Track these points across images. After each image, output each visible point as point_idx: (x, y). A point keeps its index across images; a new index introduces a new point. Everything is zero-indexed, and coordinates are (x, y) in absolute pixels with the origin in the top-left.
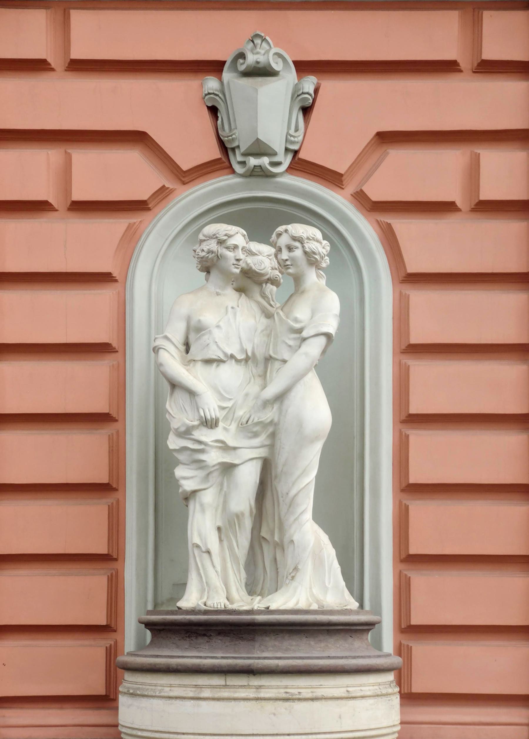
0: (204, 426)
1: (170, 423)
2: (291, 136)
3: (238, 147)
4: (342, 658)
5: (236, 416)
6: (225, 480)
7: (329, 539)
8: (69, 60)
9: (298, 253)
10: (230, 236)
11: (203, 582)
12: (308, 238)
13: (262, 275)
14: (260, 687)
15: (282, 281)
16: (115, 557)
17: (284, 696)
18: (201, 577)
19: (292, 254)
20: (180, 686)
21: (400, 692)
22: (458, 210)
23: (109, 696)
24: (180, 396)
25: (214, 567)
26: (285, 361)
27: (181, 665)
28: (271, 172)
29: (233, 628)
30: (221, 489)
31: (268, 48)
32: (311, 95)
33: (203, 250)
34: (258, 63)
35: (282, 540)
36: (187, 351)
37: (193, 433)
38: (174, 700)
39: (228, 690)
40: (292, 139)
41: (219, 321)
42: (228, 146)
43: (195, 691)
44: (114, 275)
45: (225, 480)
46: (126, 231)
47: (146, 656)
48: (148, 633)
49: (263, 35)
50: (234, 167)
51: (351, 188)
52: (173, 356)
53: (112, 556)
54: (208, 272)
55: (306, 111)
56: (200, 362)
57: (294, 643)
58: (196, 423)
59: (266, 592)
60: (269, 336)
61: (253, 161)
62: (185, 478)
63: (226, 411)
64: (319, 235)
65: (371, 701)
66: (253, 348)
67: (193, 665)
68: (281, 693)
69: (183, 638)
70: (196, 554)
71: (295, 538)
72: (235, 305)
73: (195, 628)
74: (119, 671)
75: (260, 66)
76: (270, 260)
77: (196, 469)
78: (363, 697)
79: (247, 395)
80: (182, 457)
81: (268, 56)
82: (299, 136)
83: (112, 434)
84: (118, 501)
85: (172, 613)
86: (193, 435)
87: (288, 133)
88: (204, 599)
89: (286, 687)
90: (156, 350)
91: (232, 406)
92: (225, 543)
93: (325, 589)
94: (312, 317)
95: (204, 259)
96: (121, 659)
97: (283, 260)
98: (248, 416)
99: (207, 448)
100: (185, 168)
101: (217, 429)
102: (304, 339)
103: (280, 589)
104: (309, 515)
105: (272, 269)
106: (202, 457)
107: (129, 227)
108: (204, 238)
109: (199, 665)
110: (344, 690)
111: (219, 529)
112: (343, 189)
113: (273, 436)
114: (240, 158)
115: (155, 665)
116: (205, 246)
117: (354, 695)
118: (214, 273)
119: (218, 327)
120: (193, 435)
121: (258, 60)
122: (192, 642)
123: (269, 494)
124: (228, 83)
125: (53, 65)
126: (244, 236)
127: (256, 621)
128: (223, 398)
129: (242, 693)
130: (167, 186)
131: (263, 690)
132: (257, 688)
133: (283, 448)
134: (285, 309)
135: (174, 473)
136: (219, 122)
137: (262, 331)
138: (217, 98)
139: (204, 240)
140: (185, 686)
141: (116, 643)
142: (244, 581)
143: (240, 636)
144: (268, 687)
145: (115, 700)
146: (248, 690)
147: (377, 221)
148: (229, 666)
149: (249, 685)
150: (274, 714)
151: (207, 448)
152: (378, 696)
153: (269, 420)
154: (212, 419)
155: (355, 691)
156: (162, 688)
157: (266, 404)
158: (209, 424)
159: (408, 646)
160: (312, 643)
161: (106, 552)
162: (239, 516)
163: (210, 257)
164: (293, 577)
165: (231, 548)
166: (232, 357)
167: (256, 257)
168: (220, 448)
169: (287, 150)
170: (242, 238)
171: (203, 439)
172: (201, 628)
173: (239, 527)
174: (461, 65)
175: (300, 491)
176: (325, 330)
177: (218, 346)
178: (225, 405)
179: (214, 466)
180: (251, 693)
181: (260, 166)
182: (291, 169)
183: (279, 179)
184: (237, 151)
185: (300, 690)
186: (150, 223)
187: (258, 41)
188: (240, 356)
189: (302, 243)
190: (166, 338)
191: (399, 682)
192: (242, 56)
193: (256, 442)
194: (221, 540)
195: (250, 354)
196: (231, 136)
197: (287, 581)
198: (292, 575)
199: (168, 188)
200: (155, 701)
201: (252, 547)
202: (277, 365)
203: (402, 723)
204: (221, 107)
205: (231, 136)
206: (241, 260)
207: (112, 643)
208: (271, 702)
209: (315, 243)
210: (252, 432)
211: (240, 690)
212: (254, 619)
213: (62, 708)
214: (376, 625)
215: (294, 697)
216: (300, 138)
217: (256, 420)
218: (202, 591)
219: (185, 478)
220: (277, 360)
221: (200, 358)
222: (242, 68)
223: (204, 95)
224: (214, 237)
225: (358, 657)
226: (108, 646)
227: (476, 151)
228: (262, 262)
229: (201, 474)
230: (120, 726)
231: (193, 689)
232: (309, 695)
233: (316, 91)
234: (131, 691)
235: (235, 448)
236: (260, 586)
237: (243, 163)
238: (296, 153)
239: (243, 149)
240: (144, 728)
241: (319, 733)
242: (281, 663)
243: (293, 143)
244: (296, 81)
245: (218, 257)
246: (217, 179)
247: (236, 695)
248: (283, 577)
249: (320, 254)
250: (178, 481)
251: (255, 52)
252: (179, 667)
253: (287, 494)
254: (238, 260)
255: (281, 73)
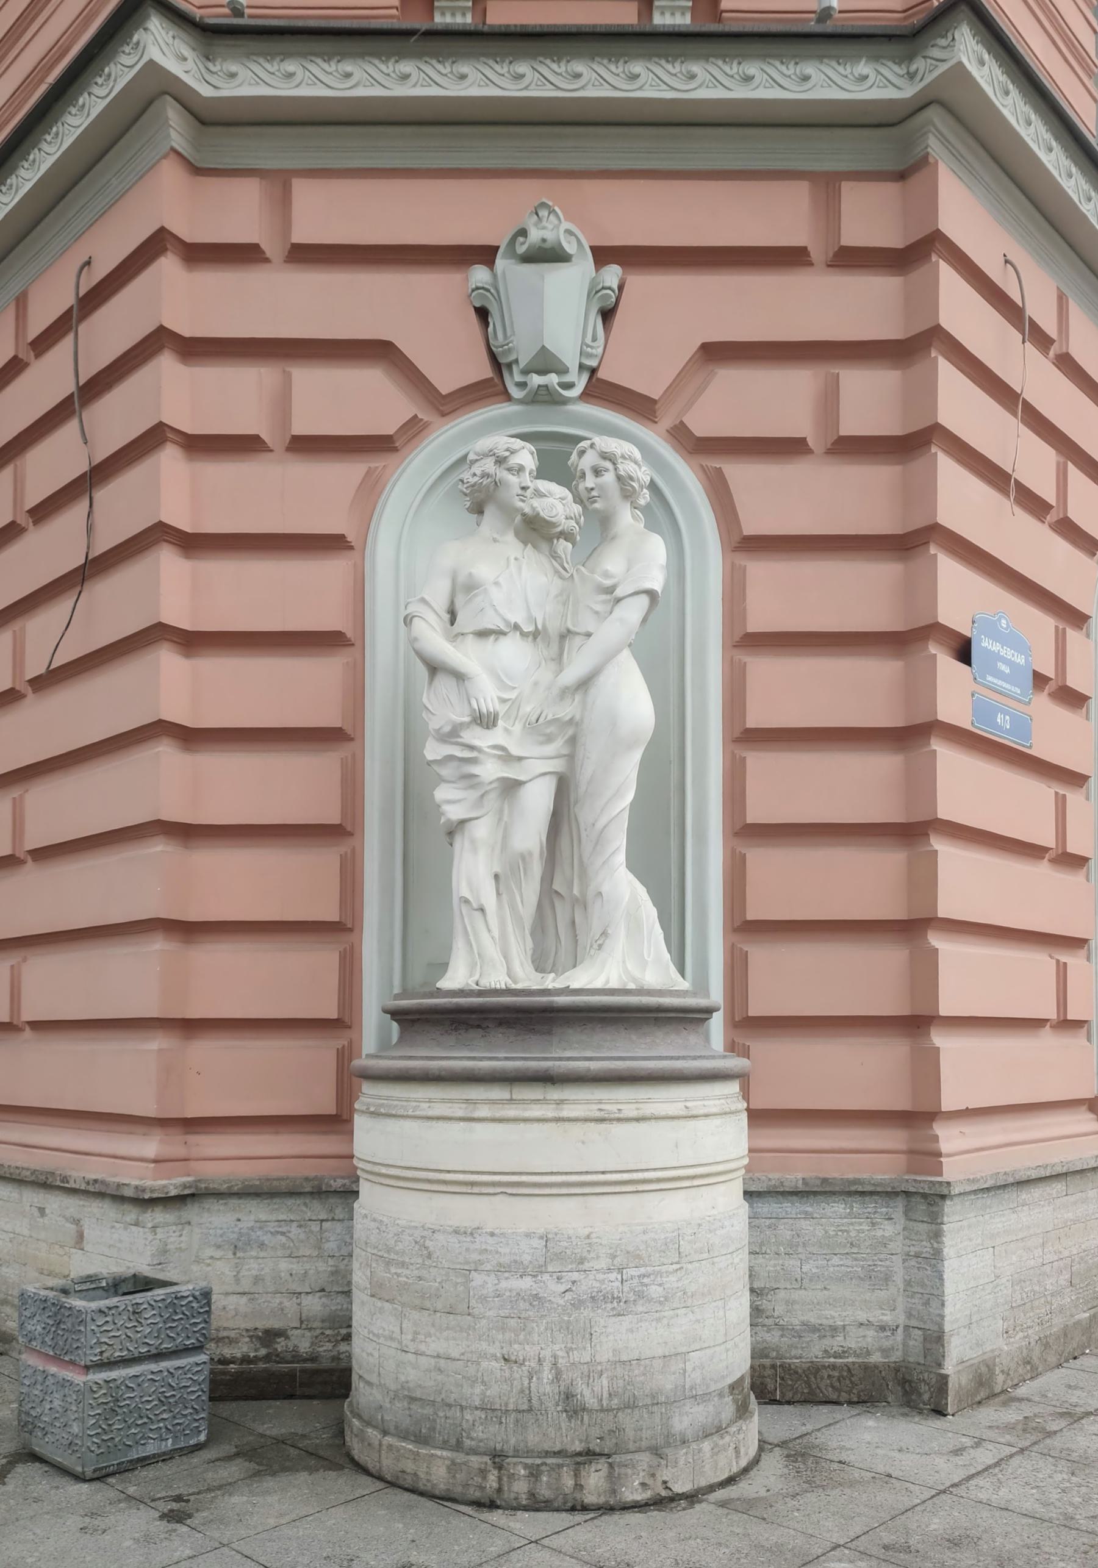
0: (478, 724)
1: (428, 724)
2: (588, 346)
3: (516, 361)
4: (678, 1058)
5: (520, 713)
6: (506, 806)
7: (648, 892)
8: (289, 246)
9: (609, 478)
10: (513, 452)
11: (473, 952)
12: (623, 457)
13: (553, 525)
14: (561, 1102)
15: (578, 538)
16: (349, 926)
17: (598, 1114)
18: (471, 946)
19: (599, 480)
20: (443, 1101)
21: (748, 1110)
22: (810, 451)
23: (340, 1116)
24: (444, 685)
25: (489, 931)
26: (589, 635)
27: (445, 1070)
28: (561, 395)
29: (520, 1016)
30: (500, 820)
31: (556, 222)
32: (613, 291)
33: (475, 475)
34: (544, 240)
35: (583, 893)
36: (452, 622)
37: (462, 734)
38: (434, 1122)
39: (514, 1106)
40: (589, 350)
41: (498, 577)
42: (503, 360)
43: (466, 1108)
44: (349, 540)
45: (506, 806)
46: (364, 479)
47: (393, 1058)
48: (395, 1025)
49: (550, 203)
50: (510, 391)
51: (667, 422)
52: (431, 625)
53: (345, 925)
54: (481, 512)
55: (607, 315)
56: (471, 636)
57: (609, 1038)
58: (467, 719)
59: (560, 969)
60: (565, 604)
61: (536, 380)
62: (449, 802)
63: (509, 703)
64: (637, 454)
65: (717, 1121)
66: (544, 619)
67: (464, 1069)
68: (593, 1111)
69: (446, 1032)
70: (464, 912)
71: (605, 889)
72: (519, 556)
73: (464, 1016)
74: (355, 1080)
75: (547, 245)
76: (564, 505)
77: (465, 789)
78: (706, 1116)
79: (536, 684)
80: (446, 772)
81: (558, 231)
82: (598, 347)
83: (346, 757)
84: (353, 851)
85: (431, 995)
86: (461, 737)
87: (583, 343)
88: (476, 978)
89: (600, 1102)
90: (408, 620)
91: (516, 698)
92: (504, 897)
93: (643, 964)
94: (628, 571)
95: (476, 488)
96: (357, 1063)
97: (586, 488)
98: (539, 712)
99: (481, 756)
100: (444, 390)
101: (495, 729)
102: (618, 600)
103: (582, 962)
104: (621, 858)
105: (567, 518)
106: (475, 770)
107: (369, 473)
108: (476, 457)
109: (473, 1070)
110: (681, 1105)
111: (496, 877)
112: (656, 422)
113: (573, 741)
114: (518, 378)
115: (408, 1070)
116: (477, 469)
117: (695, 1113)
118: (490, 511)
119: (496, 583)
120: (461, 737)
121: (545, 237)
122: (460, 1037)
123: (565, 829)
124: (504, 273)
125: (268, 254)
126: (532, 454)
127: (555, 1005)
128: (503, 686)
129: (536, 1112)
130: (420, 416)
131: (565, 1106)
132: (558, 1104)
133: (588, 758)
134: (586, 565)
135: (433, 795)
136: (491, 329)
137: (557, 596)
138: (488, 294)
139: (477, 460)
140: (451, 1101)
141: (351, 1043)
142: (529, 953)
143: (532, 1027)
144: (575, 1102)
145: (350, 1121)
146: (545, 1106)
147: (702, 466)
148: (517, 1070)
149: (545, 1099)
150: (583, 1143)
151: (481, 756)
152: (725, 1113)
153: (567, 718)
154: (489, 713)
155: (697, 1107)
156: (418, 1104)
157: (565, 693)
158: (485, 720)
159: (744, 1045)
160: (634, 1037)
161: (338, 920)
162: (524, 857)
163: (484, 483)
164: (600, 946)
165: (513, 907)
166: (516, 627)
167: (545, 499)
168: (500, 757)
169: (581, 367)
170: (530, 456)
171: (477, 743)
172: (474, 1016)
173: (525, 873)
174: (811, 255)
175: (611, 820)
176: (648, 585)
177: (496, 610)
178: (505, 696)
179: (491, 783)
180: (549, 1112)
181: (546, 386)
182: (587, 395)
183: (571, 407)
184: (514, 367)
185: (620, 1106)
186: (397, 468)
187: (544, 213)
188: (528, 628)
189: (614, 464)
190: (423, 601)
191: (746, 1094)
192: (523, 233)
193: (550, 749)
194: (498, 894)
195: (540, 627)
196: (507, 344)
197: (592, 952)
198: (599, 942)
199: (422, 420)
200: (407, 1124)
201: (540, 906)
202: (578, 640)
203: (751, 1151)
204: (494, 309)
205: (507, 344)
206: (528, 488)
207: (346, 1043)
208: (579, 1124)
209: (633, 464)
210: (545, 735)
211: (534, 1106)
212: (552, 1002)
213: (277, 1133)
214: (714, 1014)
215: (612, 1116)
216: (600, 350)
217: (550, 717)
218: (472, 967)
219: (449, 802)
220: (579, 634)
221: (471, 630)
222: (521, 249)
223: (470, 290)
224: (490, 453)
225: (700, 1057)
226: (340, 1047)
227: (832, 371)
228: (553, 506)
229: (473, 795)
230: (355, 1159)
231: (464, 1106)
232: (634, 1114)
233: (621, 288)
234: (372, 1109)
235: (520, 759)
236: (551, 961)
237: (522, 385)
238: (593, 371)
239: (522, 364)
240: (391, 1162)
241: (647, 1170)
242: (594, 1066)
243: (590, 356)
244: (594, 274)
245: (496, 483)
246: (486, 409)
247: (527, 1114)
248: (585, 948)
249: (638, 479)
250: (439, 806)
251: (540, 226)
252: (443, 1073)
253: (594, 825)
254: (524, 488)
255: (573, 259)
